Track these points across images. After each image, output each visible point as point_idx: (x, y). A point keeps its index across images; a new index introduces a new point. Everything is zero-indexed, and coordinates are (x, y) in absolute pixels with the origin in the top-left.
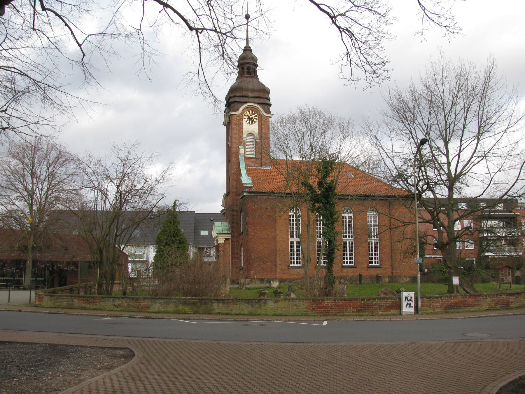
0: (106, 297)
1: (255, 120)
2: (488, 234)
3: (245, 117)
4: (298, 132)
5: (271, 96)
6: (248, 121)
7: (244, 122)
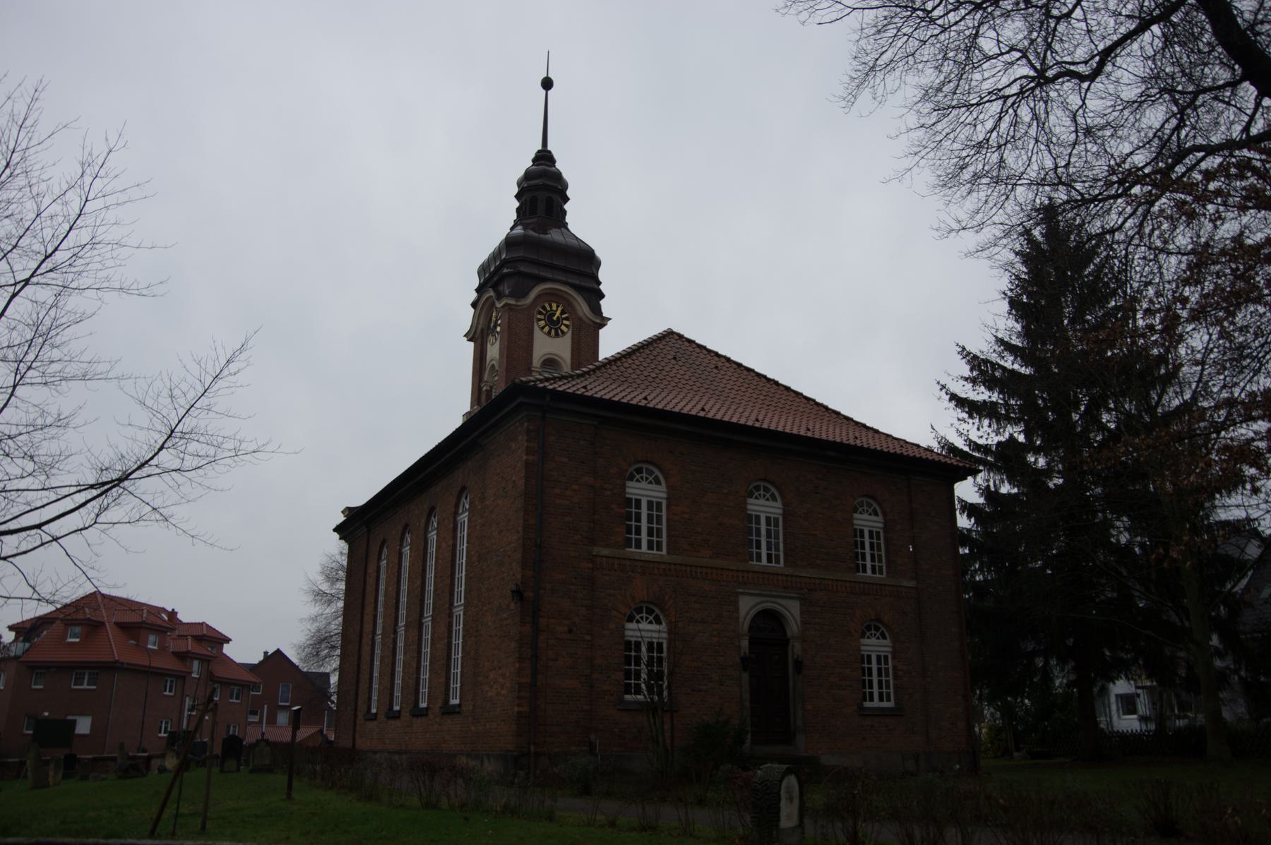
0: (1027, 85)
3: (539, 316)
5: (602, 274)
6: (547, 329)
7: (536, 329)
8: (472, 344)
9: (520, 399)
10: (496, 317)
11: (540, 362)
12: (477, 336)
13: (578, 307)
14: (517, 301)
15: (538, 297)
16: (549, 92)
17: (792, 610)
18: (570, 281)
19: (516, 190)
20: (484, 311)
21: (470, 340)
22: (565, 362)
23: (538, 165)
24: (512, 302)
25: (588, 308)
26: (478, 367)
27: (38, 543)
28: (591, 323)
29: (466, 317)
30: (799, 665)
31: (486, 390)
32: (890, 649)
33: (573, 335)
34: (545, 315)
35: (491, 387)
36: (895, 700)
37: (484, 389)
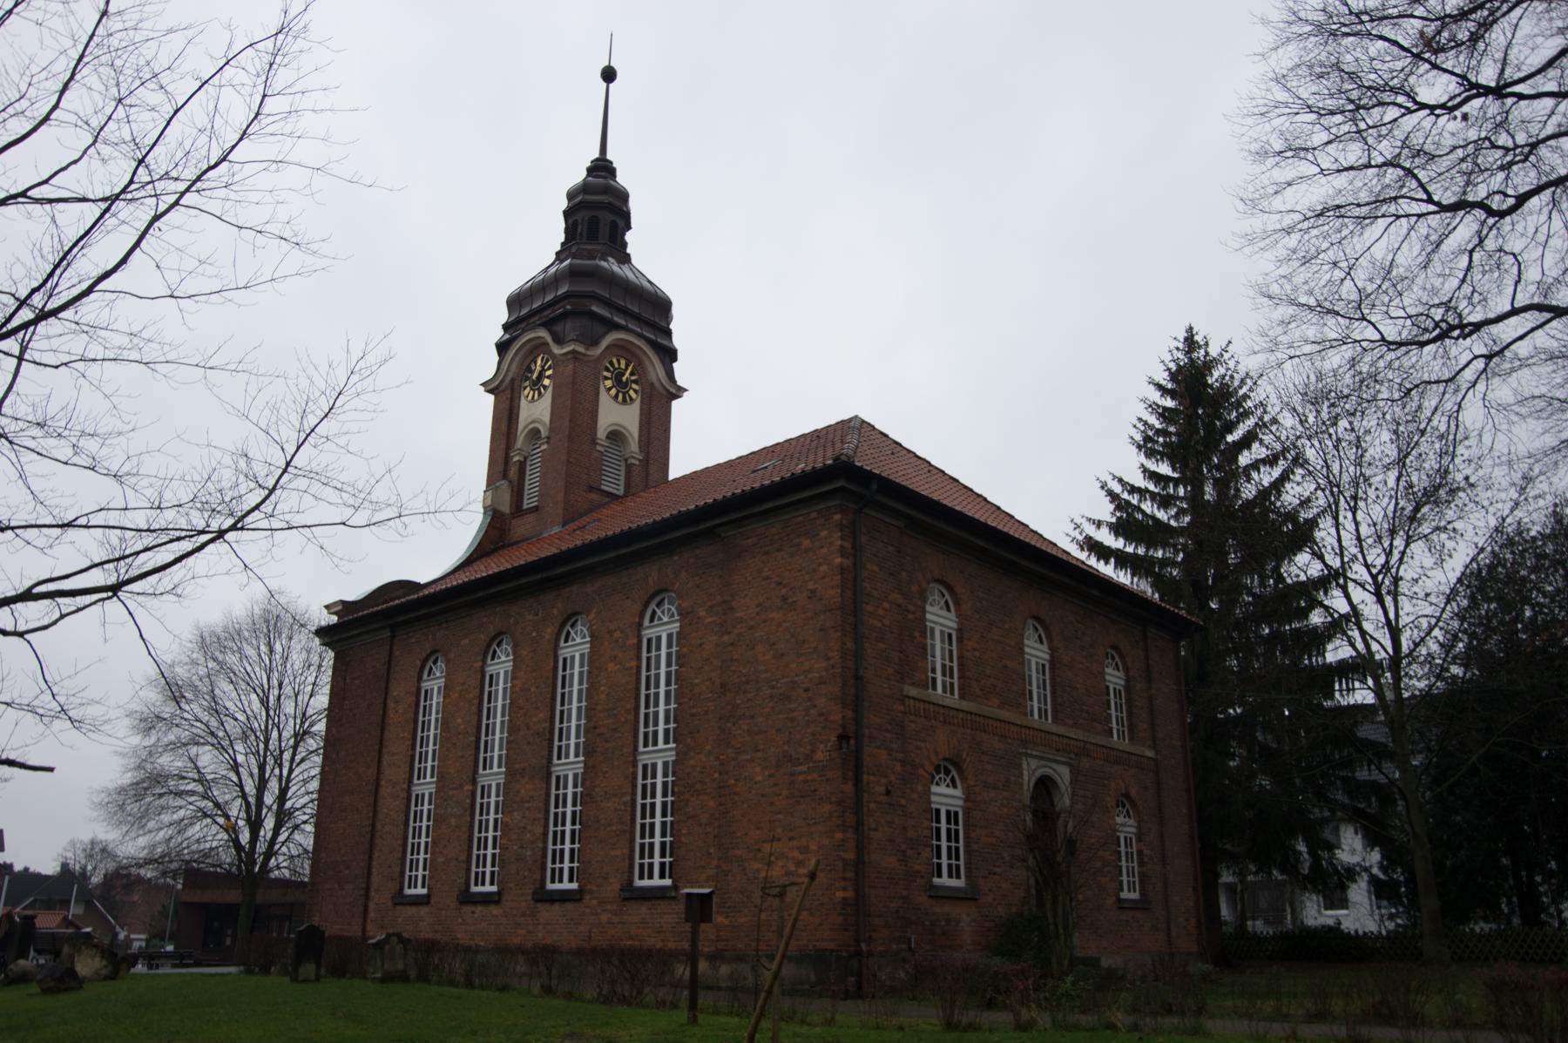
1: (546, 382)
2: (1136, 547)
3: (606, 374)
4: (237, 637)
6: (613, 392)
7: (602, 391)
8: (491, 398)
9: (839, 484)
10: (543, 367)
11: (606, 433)
12: (502, 388)
13: (650, 369)
14: (587, 349)
15: (608, 347)
16: (611, 85)
17: (1062, 775)
18: (645, 333)
19: (564, 204)
20: (517, 359)
21: (490, 391)
22: (631, 435)
23: (594, 177)
24: (581, 349)
25: (664, 372)
26: (504, 428)
27: (57, 615)
28: (664, 392)
29: (488, 364)
30: (1071, 844)
31: (519, 461)
32: (1134, 830)
33: (642, 402)
34: (612, 373)
35: (526, 458)
36: (1140, 891)
37: (516, 459)
